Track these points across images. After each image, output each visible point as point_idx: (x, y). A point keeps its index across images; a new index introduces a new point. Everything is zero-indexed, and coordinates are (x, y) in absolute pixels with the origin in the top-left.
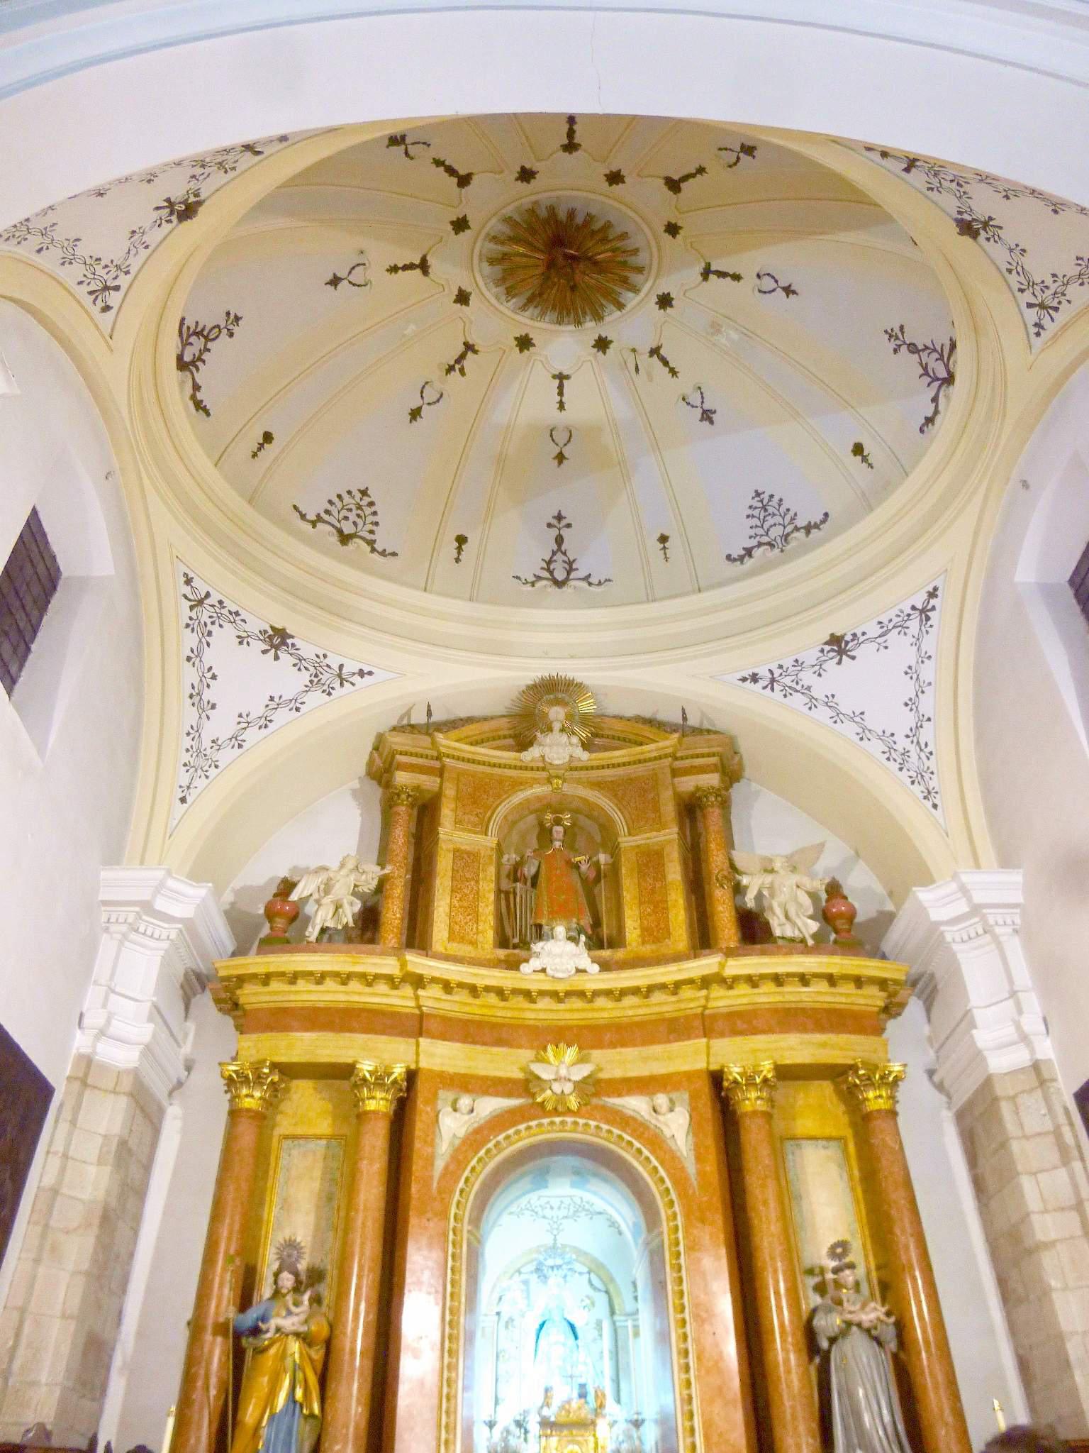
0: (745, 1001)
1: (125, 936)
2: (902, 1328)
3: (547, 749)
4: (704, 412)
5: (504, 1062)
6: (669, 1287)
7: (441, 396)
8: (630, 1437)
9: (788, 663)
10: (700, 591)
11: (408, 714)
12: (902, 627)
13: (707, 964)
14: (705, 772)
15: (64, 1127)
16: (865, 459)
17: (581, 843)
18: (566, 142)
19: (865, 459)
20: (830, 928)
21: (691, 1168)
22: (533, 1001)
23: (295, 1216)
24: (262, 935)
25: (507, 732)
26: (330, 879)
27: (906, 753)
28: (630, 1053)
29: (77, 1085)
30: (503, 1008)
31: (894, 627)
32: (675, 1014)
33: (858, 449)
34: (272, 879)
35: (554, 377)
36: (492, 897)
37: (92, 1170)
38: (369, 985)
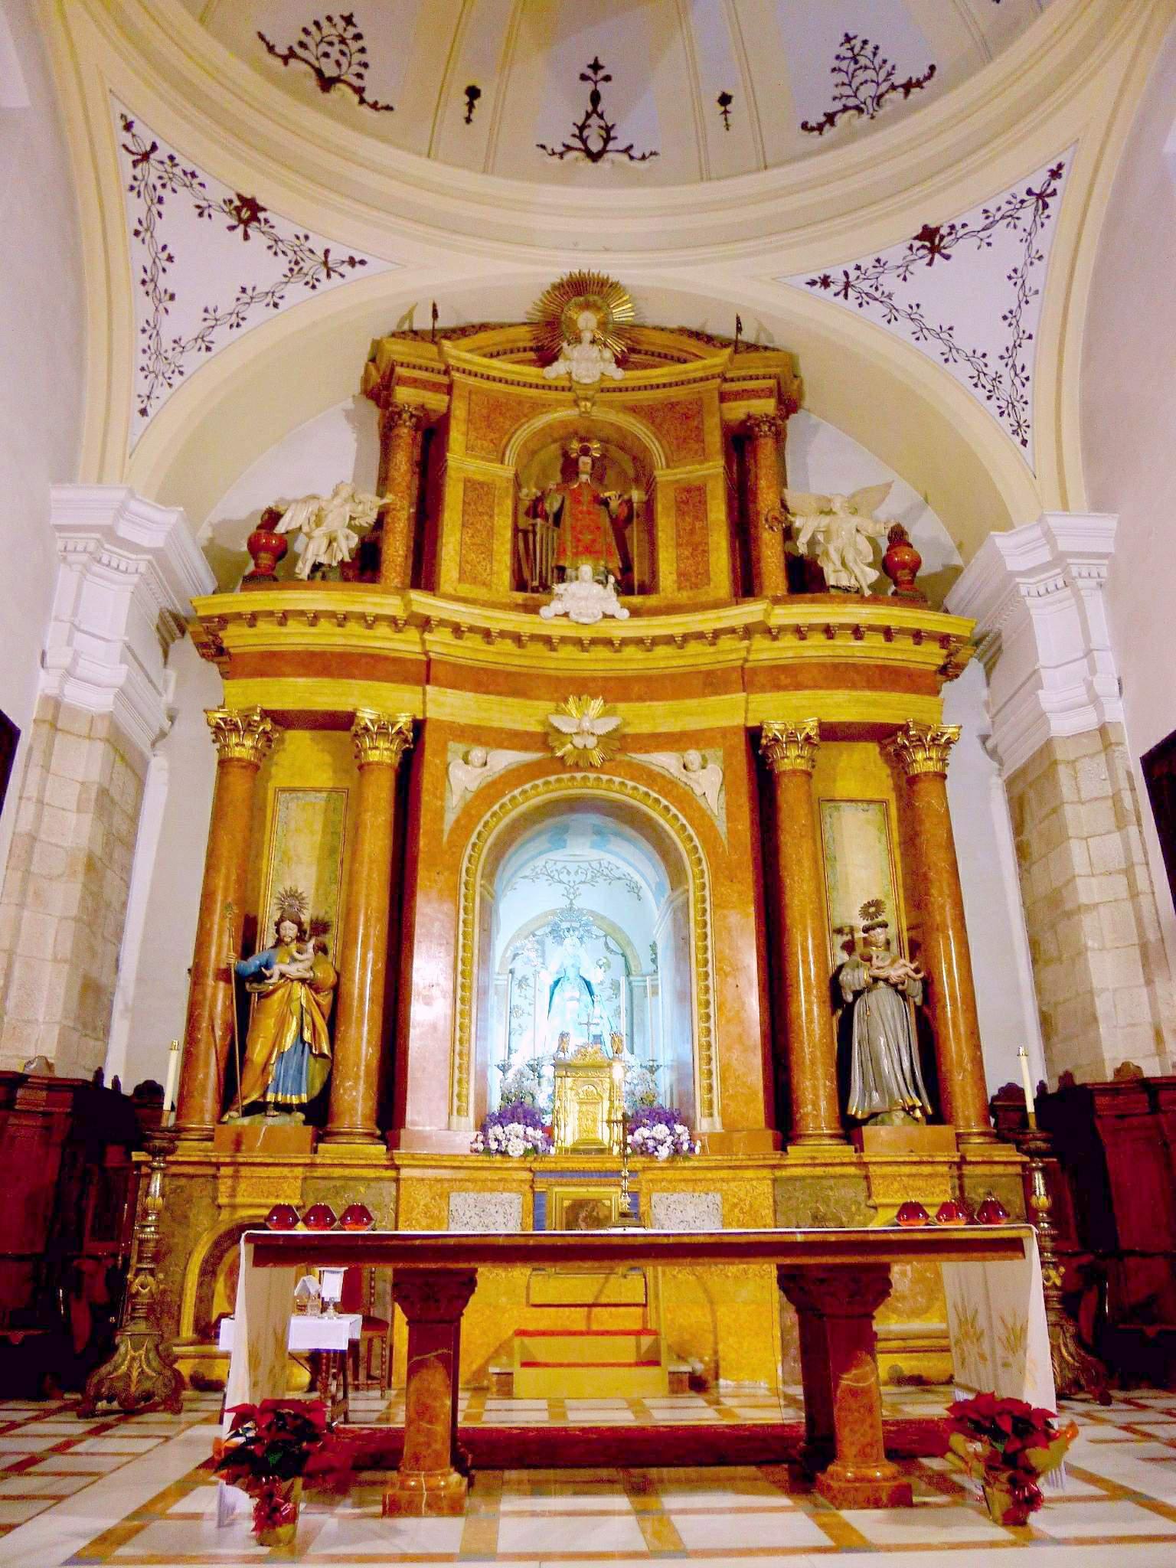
0: (790, 654)
1: (86, 568)
2: (929, 985)
5: (521, 714)
6: (693, 943)
8: (644, 1080)
9: (867, 263)
10: (766, 167)
11: (409, 316)
12: (1012, 217)
13: (752, 611)
15: (35, 774)
17: (611, 475)
20: (890, 580)
21: (722, 827)
22: (553, 649)
23: (297, 866)
24: (247, 572)
25: (531, 344)
26: (321, 509)
27: (998, 378)
28: (659, 707)
29: (45, 729)
30: (520, 656)
32: (710, 667)
34: (253, 514)
36: (509, 534)
37: (72, 818)
38: (370, 627)
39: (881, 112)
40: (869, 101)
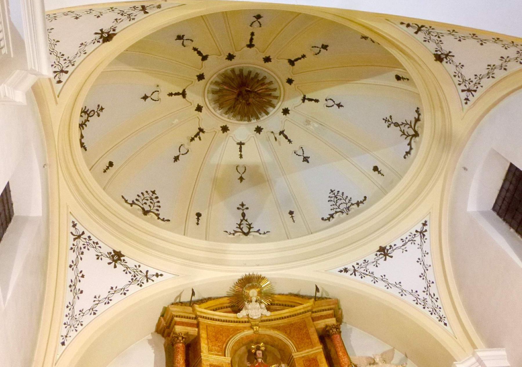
3: (250, 311)
4: (304, 157)
7: (188, 151)
9: (361, 262)
11: (180, 296)
12: (413, 241)
14: (328, 318)
16: (379, 172)
18: (249, 43)
19: (379, 172)
25: (228, 305)
27: (425, 300)
31: (409, 241)
33: (376, 169)
35: (238, 144)
39: (350, 212)
40: (345, 210)
